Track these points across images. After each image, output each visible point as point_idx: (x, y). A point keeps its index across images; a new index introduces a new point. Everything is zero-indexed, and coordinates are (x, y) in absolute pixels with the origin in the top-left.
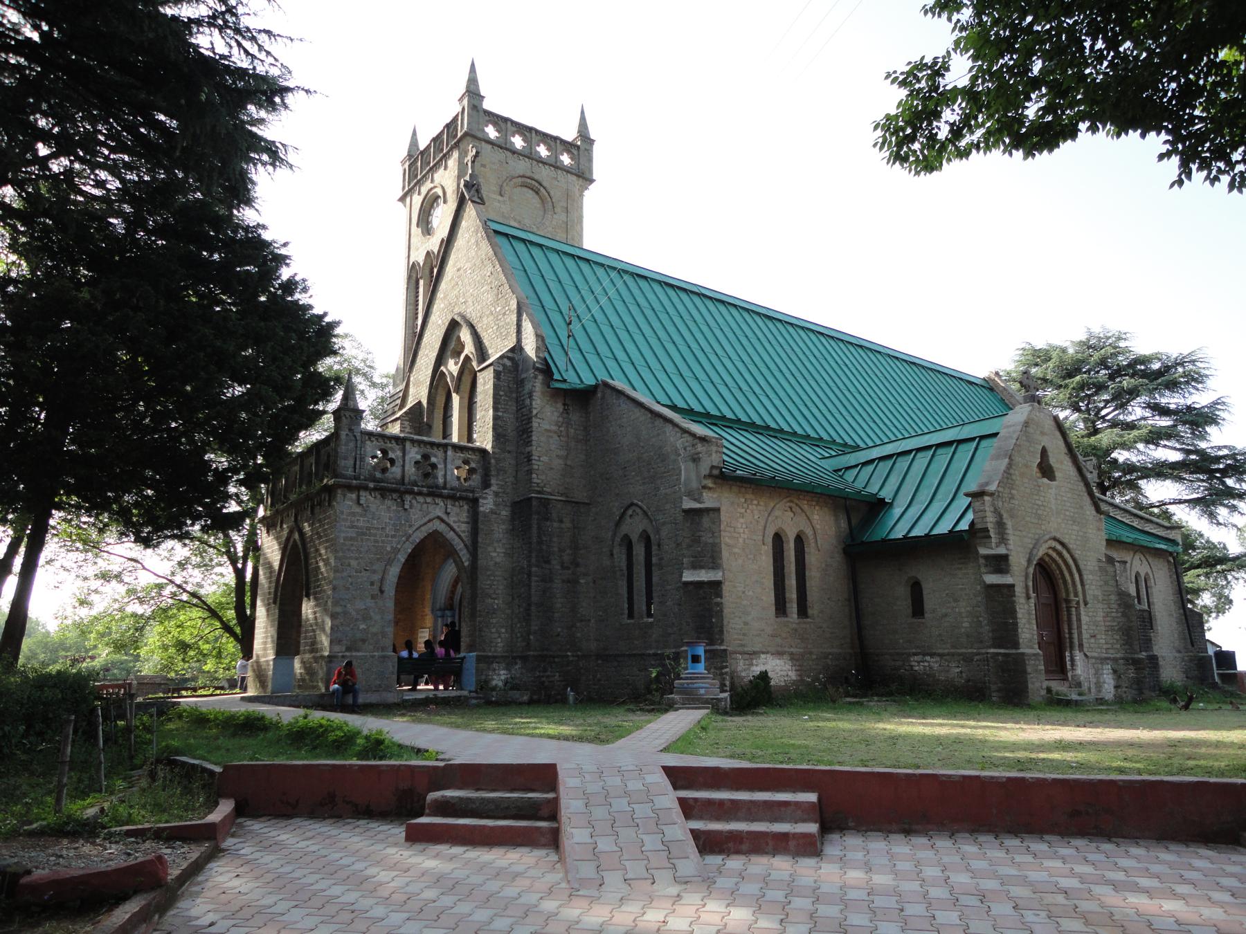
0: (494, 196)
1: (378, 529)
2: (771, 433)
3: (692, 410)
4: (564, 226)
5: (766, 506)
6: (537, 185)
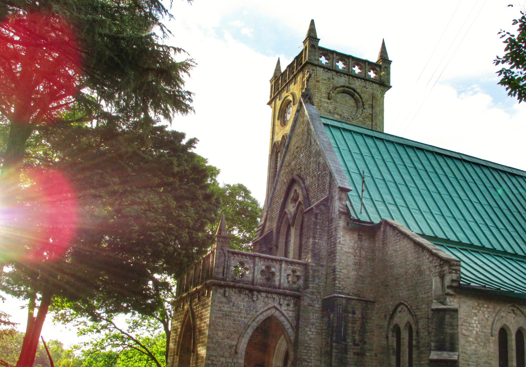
0: (324, 100)
1: (236, 312)
2: (508, 256)
3: (449, 240)
4: (370, 116)
5: (494, 308)
6: (352, 91)
